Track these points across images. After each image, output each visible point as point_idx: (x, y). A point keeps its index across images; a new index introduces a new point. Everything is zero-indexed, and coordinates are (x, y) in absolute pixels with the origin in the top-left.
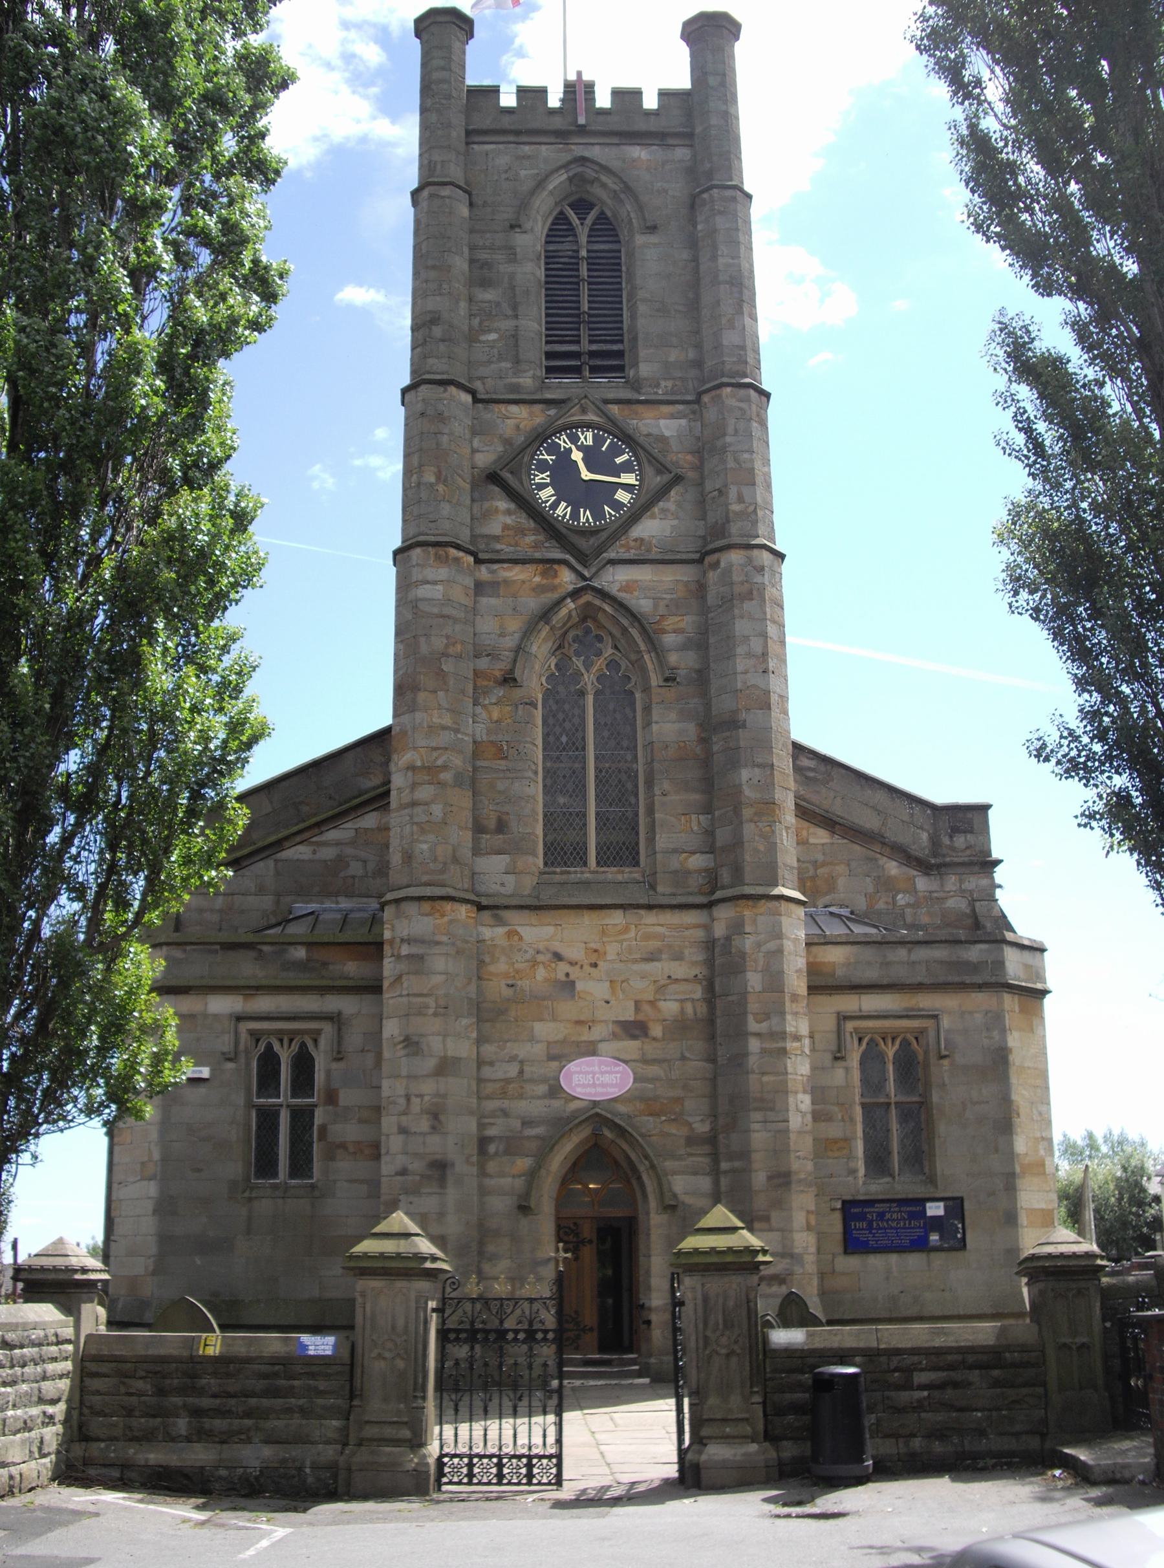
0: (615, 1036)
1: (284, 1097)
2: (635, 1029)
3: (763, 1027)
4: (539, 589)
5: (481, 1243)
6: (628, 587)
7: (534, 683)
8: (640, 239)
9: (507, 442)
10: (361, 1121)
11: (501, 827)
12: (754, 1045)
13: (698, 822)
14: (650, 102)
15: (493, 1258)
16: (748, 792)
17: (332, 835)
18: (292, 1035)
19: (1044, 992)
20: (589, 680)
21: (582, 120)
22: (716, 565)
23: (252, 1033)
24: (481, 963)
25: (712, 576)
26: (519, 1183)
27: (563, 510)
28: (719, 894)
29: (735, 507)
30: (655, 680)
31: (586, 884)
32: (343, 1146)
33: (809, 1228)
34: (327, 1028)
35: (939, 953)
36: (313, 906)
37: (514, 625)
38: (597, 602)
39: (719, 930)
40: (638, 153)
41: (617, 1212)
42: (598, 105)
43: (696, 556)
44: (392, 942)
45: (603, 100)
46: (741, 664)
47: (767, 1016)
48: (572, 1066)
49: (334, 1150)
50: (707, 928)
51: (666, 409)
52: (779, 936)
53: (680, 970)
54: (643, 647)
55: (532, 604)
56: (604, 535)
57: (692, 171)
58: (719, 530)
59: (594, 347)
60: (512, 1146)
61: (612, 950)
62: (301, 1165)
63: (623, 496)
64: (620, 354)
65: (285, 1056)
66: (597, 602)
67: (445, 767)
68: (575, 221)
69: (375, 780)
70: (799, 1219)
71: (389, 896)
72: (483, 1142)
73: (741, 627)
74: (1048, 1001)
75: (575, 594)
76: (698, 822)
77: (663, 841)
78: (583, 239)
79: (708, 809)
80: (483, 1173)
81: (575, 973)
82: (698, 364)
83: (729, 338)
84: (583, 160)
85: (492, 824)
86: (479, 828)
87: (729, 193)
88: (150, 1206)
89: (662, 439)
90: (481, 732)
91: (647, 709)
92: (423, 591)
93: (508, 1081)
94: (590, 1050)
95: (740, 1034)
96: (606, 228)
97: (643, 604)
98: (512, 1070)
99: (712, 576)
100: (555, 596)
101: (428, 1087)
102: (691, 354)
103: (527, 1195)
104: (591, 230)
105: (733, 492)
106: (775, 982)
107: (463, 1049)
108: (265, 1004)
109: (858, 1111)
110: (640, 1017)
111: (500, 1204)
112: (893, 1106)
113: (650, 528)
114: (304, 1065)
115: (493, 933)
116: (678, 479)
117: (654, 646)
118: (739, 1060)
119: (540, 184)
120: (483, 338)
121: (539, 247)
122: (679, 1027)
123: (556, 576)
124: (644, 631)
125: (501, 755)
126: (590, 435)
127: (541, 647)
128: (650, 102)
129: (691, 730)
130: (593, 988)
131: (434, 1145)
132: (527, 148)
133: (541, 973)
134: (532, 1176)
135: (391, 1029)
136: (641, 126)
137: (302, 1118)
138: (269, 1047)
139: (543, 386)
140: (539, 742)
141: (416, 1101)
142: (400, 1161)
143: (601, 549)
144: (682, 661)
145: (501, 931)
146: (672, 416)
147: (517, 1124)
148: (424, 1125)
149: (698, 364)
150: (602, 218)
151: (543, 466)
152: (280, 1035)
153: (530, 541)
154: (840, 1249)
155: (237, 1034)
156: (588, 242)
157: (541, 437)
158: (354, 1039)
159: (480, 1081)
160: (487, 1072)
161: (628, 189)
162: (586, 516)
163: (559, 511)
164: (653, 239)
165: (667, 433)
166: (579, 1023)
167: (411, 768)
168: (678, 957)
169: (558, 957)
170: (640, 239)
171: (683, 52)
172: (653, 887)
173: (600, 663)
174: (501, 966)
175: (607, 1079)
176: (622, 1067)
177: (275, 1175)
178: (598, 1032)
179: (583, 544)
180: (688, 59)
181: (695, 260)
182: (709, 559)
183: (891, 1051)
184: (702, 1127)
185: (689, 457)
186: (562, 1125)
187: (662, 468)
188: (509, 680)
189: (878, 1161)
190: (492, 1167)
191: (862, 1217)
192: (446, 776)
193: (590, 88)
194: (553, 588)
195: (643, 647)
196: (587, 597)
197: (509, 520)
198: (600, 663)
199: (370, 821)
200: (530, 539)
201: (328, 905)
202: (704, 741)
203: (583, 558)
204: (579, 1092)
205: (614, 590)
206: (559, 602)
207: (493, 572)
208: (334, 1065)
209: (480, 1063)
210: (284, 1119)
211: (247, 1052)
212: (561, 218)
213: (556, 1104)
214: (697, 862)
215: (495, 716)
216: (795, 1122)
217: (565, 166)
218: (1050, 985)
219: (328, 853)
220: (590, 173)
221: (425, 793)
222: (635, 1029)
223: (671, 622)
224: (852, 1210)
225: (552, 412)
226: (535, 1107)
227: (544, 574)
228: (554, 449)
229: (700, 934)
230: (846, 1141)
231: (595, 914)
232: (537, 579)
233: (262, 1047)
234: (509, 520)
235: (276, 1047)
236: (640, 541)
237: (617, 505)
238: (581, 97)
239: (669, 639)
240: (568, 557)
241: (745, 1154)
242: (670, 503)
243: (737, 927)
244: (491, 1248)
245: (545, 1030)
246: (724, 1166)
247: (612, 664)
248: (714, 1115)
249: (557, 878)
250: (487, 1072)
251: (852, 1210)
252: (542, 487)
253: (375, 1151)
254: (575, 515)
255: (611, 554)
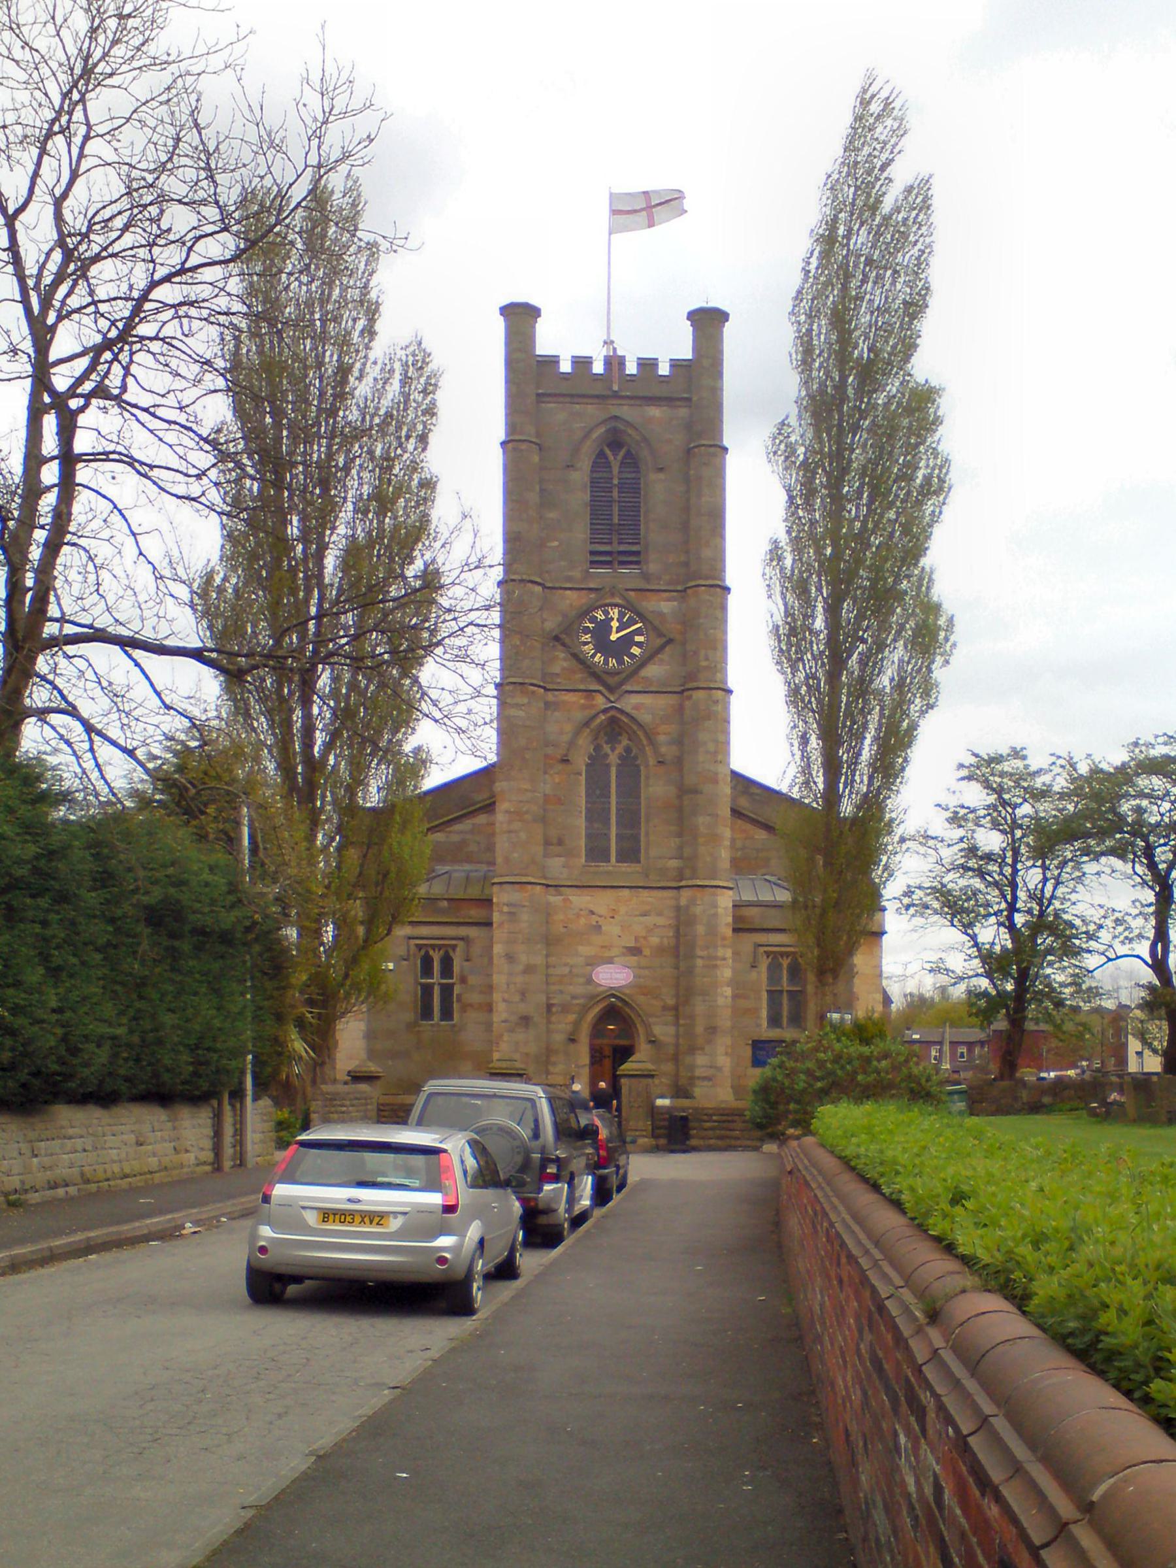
0: (624, 955)
1: (436, 979)
2: (635, 951)
3: (704, 954)
4: (584, 707)
5: (548, 1057)
6: (637, 707)
7: (580, 761)
8: (653, 476)
9: (565, 616)
10: (481, 992)
11: (560, 842)
12: (699, 962)
13: (674, 842)
14: (664, 370)
15: (554, 1064)
16: (702, 829)
17: (458, 827)
18: (440, 947)
19: (883, 933)
20: (613, 759)
21: (615, 388)
22: (689, 698)
23: (417, 945)
24: (548, 914)
25: (687, 703)
26: (569, 1028)
27: (599, 658)
28: (683, 883)
29: (704, 664)
30: (652, 761)
31: (608, 873)
32: (471, 1005)
33: (726, 1054)
34: (461, 944)
35: (620, 1004)
36: (447, 868)
37: (569, 728)
38: (619, 716)
39: (683, 902)
40: (655, 412)
41: (624, 1042)
42: (628, 372)
43: (679, 689)
44: (498, 904)
45: (631, 368)
46: (701, 758)
47: (707, 948)
48: (599, 969)
49: (464, 1008)
50: (677, 899)
51: (667, 594)
52: (716, 906)
53: (661, 921)
54: (645, 742)
55: (579, 716)
56: (624, 675)
57: (689, 426)
58: (691, 676)
59: (622, 548)
60: (565, 1009)
61: (623, 910)
62: (447, 1014)
63: (636, 651)
64: (637, 553)
65: (436, 957)
66: (619, 716)
67: (527, 812)
68: (611, 458)
69: (486, 795)
70: (721, 1050)
71: (496, 880)
72: (549, 1007)
73: (703, 736)
74: (885, 937)
75: (605, 711)
76: (674, 842)
77: (654, 852)
78: (616, 470)
79: (680, 835)
80: (549, 1022)
81: (601, 921)
82: (686, 564)
83: (706, 553)
84: (615, 418)
85: (555, 841)
86: (547, 843)
87: (712, 450)
88: (361, 1035)
89: (661, 615)
90: (548, 789)
91: (647, 778)
92: (513, 712)
93: (563, 976)
94: (610, 961)
95: (691, 956)
96: (632, 462)
97: (645, 717)
98: (566, 970)
99: (687, 703)
100: (593, 712)
101: (519, 979)
102: (683, 558)
103: (572, 1033)
104: (622, 463)
105: (702, 653)
106: (712, 931)
107: (539, 960)
108: (424, 931)
109: (765, 995)
110: (638, 945)
111: (559, 1038)
112: (785, 994)
113: (653, 671)
114: (447, 963)
115: (555, 899)
116: (670, 641)
117: (651, 742)
118: (690, 971)
119: (586, 436)
120: (549, 544)
121: (587, 479)
122: (660, 950)
123: (593, 699)
124: (646, 733)
125: (559, 802)
126: (616, 611)
127: (585, 744)
128: (664, 370)
129: (672, 790)
130: (612, 929)
131: (523, 1009)
132: (577, 406)
133: (583, 921)
134: (577, 1024)
135: (498, 949)
136: (656, 391)
137: (447, 990)
138: (427, 953)
139: (587, 575)
140: (583, 794)
141: (512, 986)
142: (504, 1016)
143: (622, 683)
144: (666, 750)
145: (561, 898)
146: (668, 600)
147: (569, 998)
148: (517, 998)
149: (686, 564)
150: (628, 454)
151: (586, 630)
152: (433, 947)
153: (579, 680)
154: (749, 1063)
155: (408, 945)
156: (620, 472)
157: (586, 613)
158: (476, 950)
159: (547, 975)
160: (551, 971)
161: (645, 440)
162: (612, 662)
163: (596, 659)
164: (661, 476)
165: (665, 611)
166: (602, 947)
167: (507, 812)
168: (660, 914)
169: (592, 913)
170: (653, 476)
171: (687, 329)
172: (647, 876)
173: (620, 749)
174: (560, 917)
175: (618, 976)
176: (627, 970)
177: (452, 1019)
178: (615, 952)
179: (612, 681)
180: (691, 337)
181: (688, 491)
182: (686, 694)
183: (785, 962)
184: (671, 1002)
185: (679, 627)
186: (593, 998)
187: (661, 635)
188: (565, 761)
189: (774, 1021)
190: (553, 1019)
191: (763, 1049)
192: (528, 817)
193: (622, 361)
194: (593, 706)
195: (645, 742)
196: (612, 713)
197: (565, 664)
198: (620, 749)
199: (482, 819)
200: (578, 676)
201: (456, 867)
202: (679, 797)
203: (611, 690)
204: (603, 982)
205: (628, 709)
206: (597, 715)
207: (555, 696)
208: (466, 964)
209: (548, 966)
210: (437, 991)
211: (415, 955)
212: (601, 454)
213: (590, 988)
214: (674, 863)
215: (557, 780)
216: (721, 1001)
217: (604, 422)
218: (887, 928)
219: (455, 838)
220: (621, 426)
221: (517, 825)
222: (635, 951)
223: (663, 728)
224: (757, 1045)
225: (593, 596)
226: (580, 990)
227: (586, 698)
228: (606, 613)
229: (673, 903)
230: (755, 1011)
231: (612, 890)
232: (582, 701)
233: (423, 952)
234: (565, 664)
235: (431, 952)
236: (646, 679)
237: (632, 656)
238: (615, 368)
239: (662, 738)
240: (601, 688)
241: (692, 1017)
242: (664, 656)
243: (692, 902)
244: (553, 1059)
245: (585, 950)
246: (681, 1022)
247: (628, 750)
248: (677, 996)
249: (592, 869)
250: (551, 971)
251: (757, 1045)
252: (586, 643)
253: (489, 1008)
254: (606, 662)
255: (629, 688)
